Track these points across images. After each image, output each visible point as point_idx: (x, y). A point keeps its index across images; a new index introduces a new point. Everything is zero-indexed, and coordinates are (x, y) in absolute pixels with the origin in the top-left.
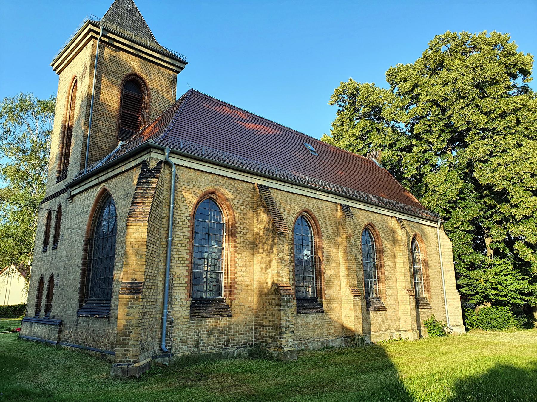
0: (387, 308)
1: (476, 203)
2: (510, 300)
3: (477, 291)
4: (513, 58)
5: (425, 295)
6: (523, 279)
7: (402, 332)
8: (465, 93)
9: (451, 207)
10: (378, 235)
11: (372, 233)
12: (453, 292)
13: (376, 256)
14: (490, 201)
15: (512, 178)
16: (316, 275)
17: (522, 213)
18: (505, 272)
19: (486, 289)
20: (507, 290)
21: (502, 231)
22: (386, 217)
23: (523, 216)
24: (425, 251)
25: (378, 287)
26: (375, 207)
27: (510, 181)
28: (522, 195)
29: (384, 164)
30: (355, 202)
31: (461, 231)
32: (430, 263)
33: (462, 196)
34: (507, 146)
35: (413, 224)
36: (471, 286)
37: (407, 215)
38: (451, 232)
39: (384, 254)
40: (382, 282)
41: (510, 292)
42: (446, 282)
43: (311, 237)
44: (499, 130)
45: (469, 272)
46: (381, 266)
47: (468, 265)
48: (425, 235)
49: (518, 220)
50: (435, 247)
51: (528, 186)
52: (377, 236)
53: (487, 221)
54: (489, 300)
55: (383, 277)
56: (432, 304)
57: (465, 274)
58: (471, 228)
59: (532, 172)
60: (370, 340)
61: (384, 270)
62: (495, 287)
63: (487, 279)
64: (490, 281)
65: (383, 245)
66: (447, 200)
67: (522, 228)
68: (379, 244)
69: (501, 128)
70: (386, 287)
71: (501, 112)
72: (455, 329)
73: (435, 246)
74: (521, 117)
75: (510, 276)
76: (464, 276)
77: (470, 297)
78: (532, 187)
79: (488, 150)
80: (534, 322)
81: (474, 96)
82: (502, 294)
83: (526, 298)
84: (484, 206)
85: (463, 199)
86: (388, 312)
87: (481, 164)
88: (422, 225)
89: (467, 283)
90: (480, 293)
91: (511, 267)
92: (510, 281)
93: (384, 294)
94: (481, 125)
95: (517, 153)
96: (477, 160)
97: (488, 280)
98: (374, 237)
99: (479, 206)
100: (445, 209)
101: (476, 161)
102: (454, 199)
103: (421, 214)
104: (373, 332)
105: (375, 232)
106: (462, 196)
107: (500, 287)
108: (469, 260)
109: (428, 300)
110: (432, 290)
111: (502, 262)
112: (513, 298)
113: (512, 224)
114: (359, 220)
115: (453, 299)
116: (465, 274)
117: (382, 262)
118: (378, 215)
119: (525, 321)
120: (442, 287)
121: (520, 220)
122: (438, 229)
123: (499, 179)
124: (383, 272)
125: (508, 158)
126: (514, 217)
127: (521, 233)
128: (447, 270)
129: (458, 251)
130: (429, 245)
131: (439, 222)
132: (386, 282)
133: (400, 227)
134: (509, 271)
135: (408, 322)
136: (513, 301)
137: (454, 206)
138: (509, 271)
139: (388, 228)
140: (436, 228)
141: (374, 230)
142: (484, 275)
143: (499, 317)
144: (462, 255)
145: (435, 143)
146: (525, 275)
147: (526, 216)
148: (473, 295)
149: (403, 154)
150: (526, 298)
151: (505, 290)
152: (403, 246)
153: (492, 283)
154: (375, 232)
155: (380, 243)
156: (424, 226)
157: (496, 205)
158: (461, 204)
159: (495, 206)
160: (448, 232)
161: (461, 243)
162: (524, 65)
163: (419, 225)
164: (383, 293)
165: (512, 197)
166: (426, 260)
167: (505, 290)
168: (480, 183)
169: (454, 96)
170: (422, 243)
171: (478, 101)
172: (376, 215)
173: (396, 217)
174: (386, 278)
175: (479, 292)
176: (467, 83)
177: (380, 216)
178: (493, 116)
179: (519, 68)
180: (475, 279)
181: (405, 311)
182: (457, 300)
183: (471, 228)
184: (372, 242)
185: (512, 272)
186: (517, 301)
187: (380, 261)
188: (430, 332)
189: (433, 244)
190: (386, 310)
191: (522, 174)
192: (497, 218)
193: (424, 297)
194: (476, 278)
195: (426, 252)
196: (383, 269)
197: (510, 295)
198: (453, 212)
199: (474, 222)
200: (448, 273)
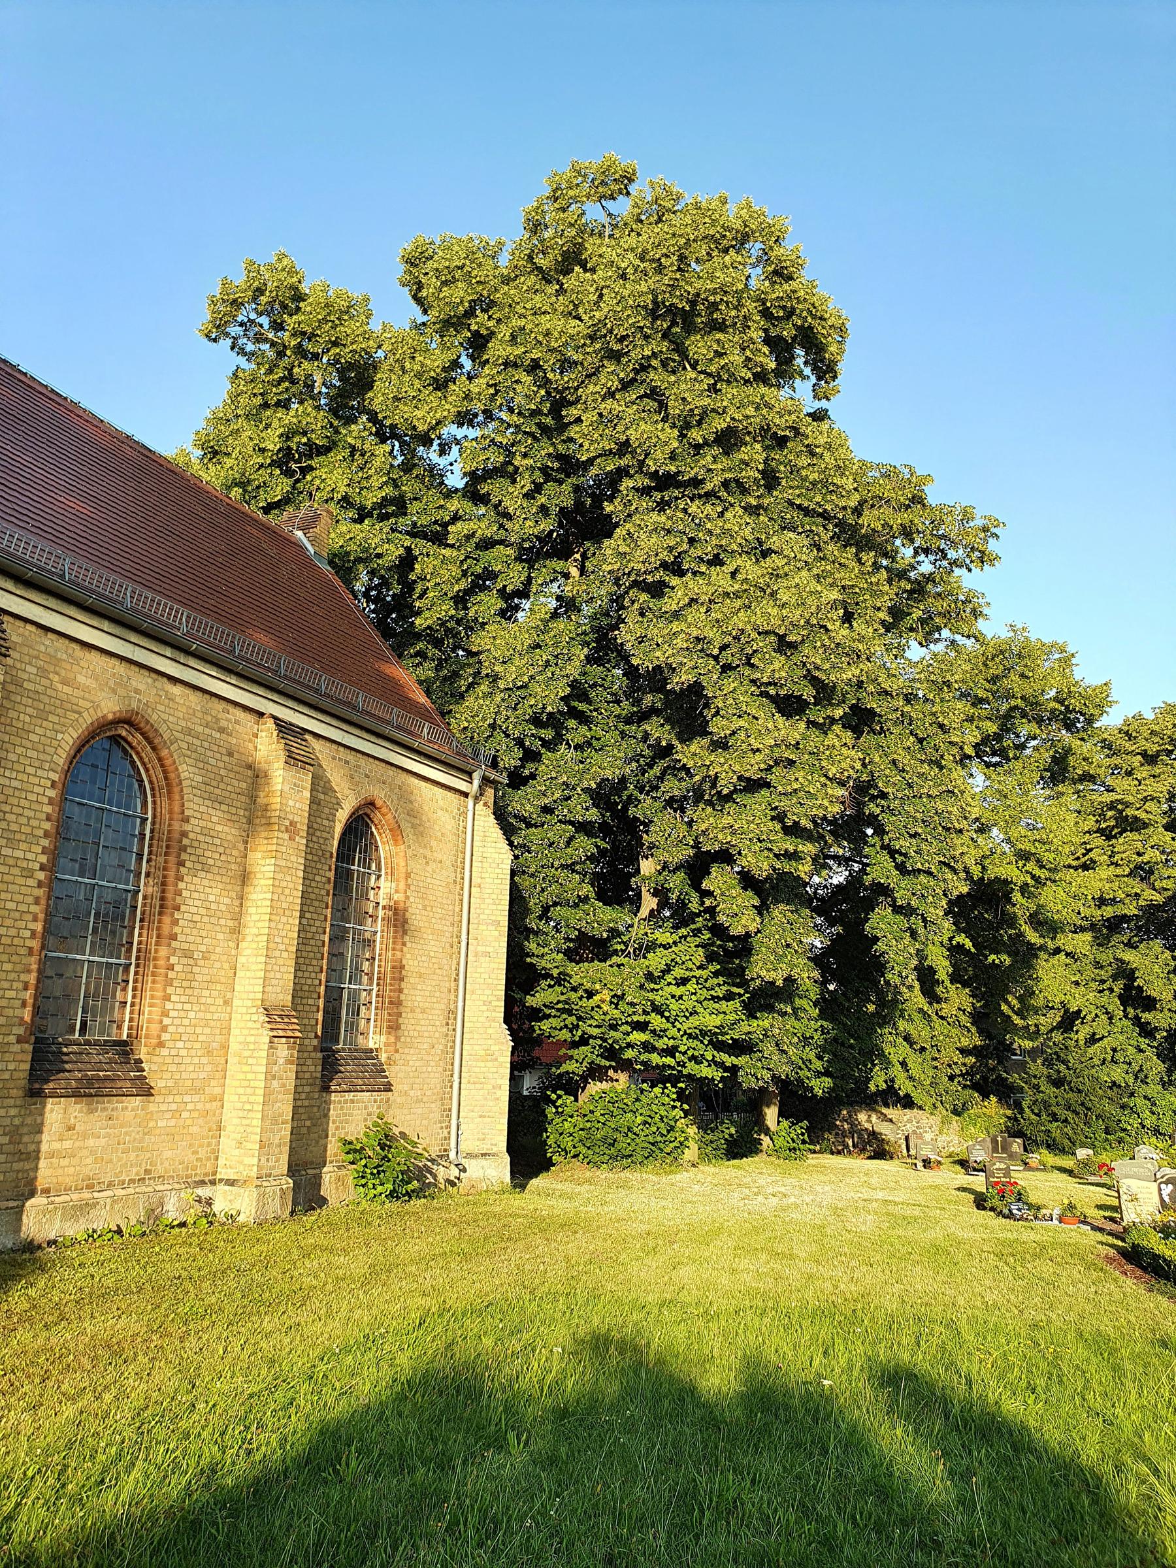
0: (158, 1083)
1: (623, 734)
2: (684, 1066)
3: (584, 1033)
4: (786, 287)
5: (374, 1039)
6: (729, 997)
7: (221, 1187)
8: (622, 339)
9: (541, 739)
10: (172, 776)
11: (144, 764)
12: (490, 1031)
13: (149, 861)
14: (659, 731)
15: (723, 648)
16: (138, 958)
17: (737, 768)
18: (678, 972)
19: (613, 1027)
20: (679, 1030)
21: (683, 830)
22: (231, 708)
23: (740, 778)
24: (403, 870)
25: (130, 993)
26: (168, 652)
27: (716, 658)
28: (744, 708)
29: (343, 564)
30: (52, 603)
31: (560, 821)
32: (416, 916)
33: (582, 707)
34: (723, 543)
35: (363, 761)
36: (570, 1012)
37: (334, 723)
38: (529, 825)
39: (184, 856)
40: (154, 974)
41: (684, 1038)
42: (473, 993)
44: (709, 486)
45: (572, 968)
46: (162, 906)
47: (571, 940)
48: (412, 814)
49: (725, 791)
50: (449, 863)
51: (765, 680)
52: (166, 778)
53: (649, 801)
54: (625, 1065)
55: (163, 951)
56: (395, 1074)
57: (555, 972)
58: (593, 815)
59: (782, 631)
60: (18, 1230)
61: (175, 922)
62: (642, 1019)
63: (619, 993)
64: (629, 998)
65: (186, 820)
66: (530, 711)
67: (732, 822)
68: (171, 812)
69: (717, 480)
70: (167, 998)
71: (724, 425)
72: (475, 1169)
73: (448, 860)
74: (782, 468)
75: (691, 986)
76: (551, 976)
77: (563, 1052)
78: (776, 684)
79: (671, 549)
80: (762, 1136)
81: (647, 352)
82: (660, 1044)
83: (729, 1060)
84: (641, 746)
85: (584, 719)
86: (156, 1104)
87: (644, 597)
88: (404, 775)
89: (559, 1002)
90: (595, 1038)
91: (700, 956)
92: (688, 1004)
93: (155, 1028)
94: (657, 461)
95: (752, 570)
96: (635, 584)
97: (621, 997)
98: (151, 782)
99: (633, 746)
100: (520, 742)
101: (631, 587)
102: (549, 709)
103: (411, 733)
104: (47, 1191)
105: (160, 759)
106: (582, 707)
107: (657, 1021)
108: (572, 922)
109: (383, 1057)
110: (406, 1020)
111: (677, 938)
112: (693, 1058)
113: (710, 809)
114: (67, 689)
115: (490, 1057)
116: (555, 972)
117: (170, 888)
118: (189, 691)
119: (731, 1135)
120: (452, 1012)
121: (732, 793)
122: (470, 801)
123: (685, 645)
124: (166, 930)
125: (720, 578)
126: (714, 781)
127: (729, 839)
128: (479, 948)
129: (543, 890)
130: (427, 852)
131: (476, 776)
132: (171, 974)
133: (282, 756)
134: (691, 970)
135: (249, 1146)
136: (691, 1068)
137: (548, 734)
138: (691, 970)
139: (230, 754)
140: (466, 795)
141: (154, 749)
142: (613, 979)
143: (645, 1123)
144: (555, 904)
145: (518, 514)
146: (734, 985)
147: (748, 779)
148: (575, 1045)
149: (419, 546)
150: (729, 1060)
151: (673, 1032)
152: (286, 836)
153: (632, 1004)
154: (160, 759)
155: (177, 809)
156: (416, 781)
157: (675, 742)
158: (576, 732)
159: (670, 747)
160: (507, 822)
161: (556, 864)
162: (814, 317)
163: (391, 772)
164: (149, 1021)
165: (717, 713)
166: (401, 906)
167: (673, 1032)
168: (635, 661)
169: (589, 356)
170: (396, 841)
171: (657, 377)
172: (177, 690)
173: (275, 718)
174: (173, 960)
175: (591, 1037)
176: (631, 302)
177: (194, 698)
178: (696, 435)
179: (799, 323)
180: (586, 991)
181: (244, 1098)
182: (501, 1059)
183: (593, 815)
184: (144, 804)
185: (698, 973)
186: (705, 1071)
187: (164, 884)
188: (363, 1181)
189: (443, 852)
190: (147, 1092)
191: (754, 635)
192: (673, 787)
193: (371, 1045)
194: (588, 986)
195: (408, 876)
196: (167, 919)
197: (683, 1048)
198: (547, 756)
199: (603, 795)
200: (482, 959)
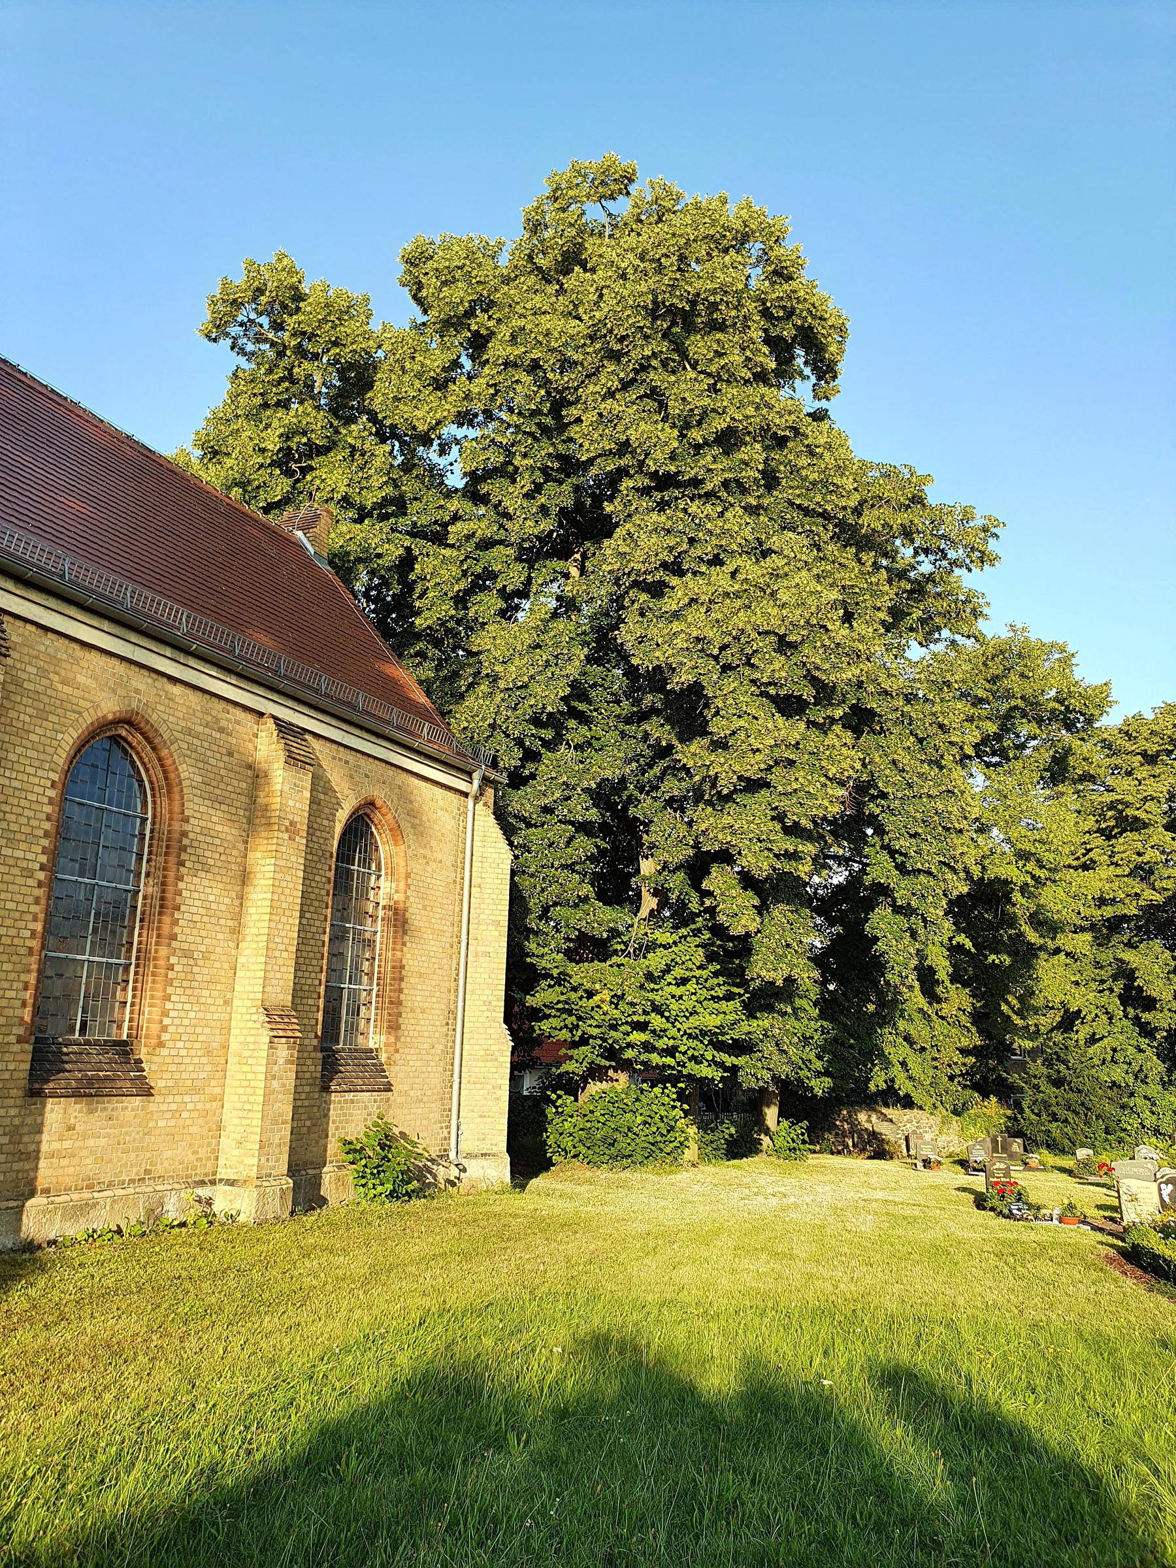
0: (158, 1083)
1: (623, 734)
2: (684, 1066)
3: (584, 1033)
4: (786, 287)
5: (374, 1039)
6: (729, 997)
7: (221, 1187)
8: (622, 339)
9: (541, 739)
10: (172, 776)
11: (144, 764)
12: (490, 1031)
13: (149, 861)
14: (659, 731)
15: (723, 648)
16: (138, 958)
17: (737, 768)
18: (678, 972)
19: (613, 1027)
20: (679, 1030)
21: (683, 830)
22: (231, 708)
23: (740, 778)
24: (403, 870)
25: (130, 993)
26: (168, 652)
27: (716, 658)
28: (744, 708)
29: (343, 564)
30: (52, 603)
31: (560, 821)
32: (416, 916)
33: (582, 707)
34: (723, 543)
35: (363, 761)
36: (570, 1012)
37: (334, 723)
38: (529, 825)
39: (184, 856)
40: (154, 974)
41: (684, 1038)
42: (473, 993)
43: (144, 820)
44: (709, 486)
45: (572, 968)
46: (162, 906)
47: (571, 940)
48: (412, 814)
49: (725, 791)
50: (449, 863)
51: (765, 680)
52: (166, 778)
53: (649, 801)
54: (625, 1065)
55: (163, 951)
56: (395, 1074)
57: (555, 972)
58: (593, 815)
59: (782, 631)
60: (18, 1230)
61: (175, 922)
62: (642, 1019)
63: (619, 993)
64: (629, 998)
65: (186, 820)
66: (530, 711)
67: (732, 822)
68: (171, 812)
69: (717, 480)
70: (167, 998)
71: (724, 425)
72: (475, 1169)
73: (448, 860)
74: (782, 468)
75: (691, 986)
76: (551, 976)
77: (563, 1052)
78: (776, 684)
79: (671, 549)
80: (762, 1136)
81: (647, 352)
82: (660, 1044)
83: (729, 1060)
84: (641, 746)
85: (584, 719)
86: (156, 1104)
87: (644, 597)
88: (404, 775)
89: (559, 1002)
90: (595, 1038)
91: (700, 956)
92: (688, 1004)
93: (155, 1028)
94: (657, 461)
95: (752, 570)
96: (635, 584)
97: (621, 997)
98: (151, 782)
99: (633, 746)
100: (520, 742)
101: (631, 587)
102: (549, 709)
103: (411, 733)
104: (47, 1191)
105: (160, 759)
106: (582, 707)
107: (657, 1021)
108: (572, 922)
109: (383, 1057)
110: (406, 1020)
111: (677, 938)
112: (693, 1058)
113: (710, 809)
114: (67, 689)
115: (490, 1057)
116: (555, 972)
117: (170, 888)
118: (189, 691)
119: (731, 1135)
120: (452, 1012)
121: (732, 793)
122: (470, 801)
123: (685, 645)
124: (166, 930)
125: (720, 578)
126: (714, 781)
127: (729, 839)
128: (479, 948)
129: (543, 890)
130: (427, 852)
131: (476, 776)
132: (171, 974)
133: (282, 756)
134: (691, 970)
135: (249, 1146)
136: (691, 1068)
137: (548, 734)
138: (691, 970)
139: (230, 754)
140: (466, 795)
141: (154, 749)
142: (613, 979)
143: (645, 1123)
144: (555, 904)
145: (518, 514)
146: (734, 985)
147: (748, 779)
148: (575, 1045)
149: (419, 546)
150: (729, 1060)
151: (673, 1032)
152: (286, 836)
153: (632, 1004)
154: (160, 759)
155: (177, 809)
156: (416, 781)
157: (675, 742)
158: (576, 732)
159: (670, 747)
160: (507, 822)
161: (556, 864)
162: (814, 317)
163: (391, 772)
164: (149, 1021)
165: (717, 713)
166: (401, 906)
167: (673, 1032)
168: (635, 661)
169: (589, 356)
170: (396, 841)
171: (657, 377)
172: (177, 690)
173: (275, 718)
174: (173, 960)
175: (591, 1037)
176: (631, 302)
177: (194, 698)
178: (696, 435)
179: (799, 323)
180: (586, 991)
181: (244, 1098)
182: (501, 1059)
183: (593, 815)
184: (144, 804)
185: (698, 973)
186: (705, 1071)
187: (164, 884)
188: (363, 1181)
189: (443, 852)
190: (147, 1092)
191: (754, 635)
192: (673, 787)
193: (371, 1045)
194: (588, 986)
195: (408, 876)
196: (167, 919)
197: (683, 1048)
198: (547, 756)
199: (603, 795)
200: (482, 959)
